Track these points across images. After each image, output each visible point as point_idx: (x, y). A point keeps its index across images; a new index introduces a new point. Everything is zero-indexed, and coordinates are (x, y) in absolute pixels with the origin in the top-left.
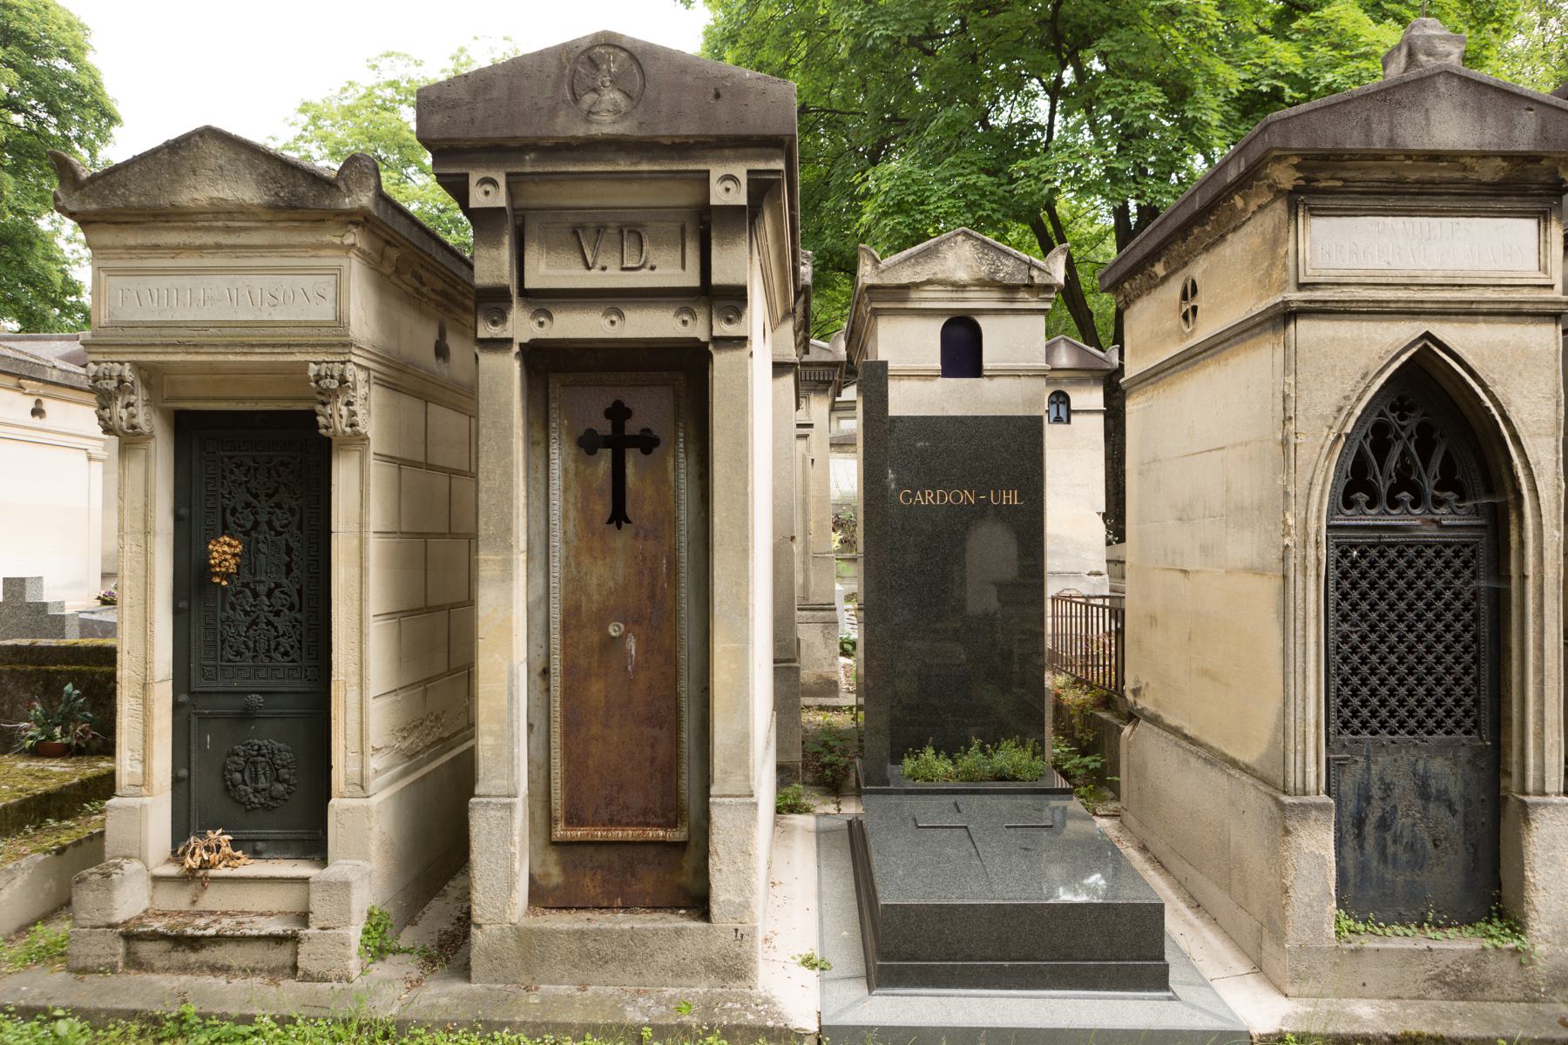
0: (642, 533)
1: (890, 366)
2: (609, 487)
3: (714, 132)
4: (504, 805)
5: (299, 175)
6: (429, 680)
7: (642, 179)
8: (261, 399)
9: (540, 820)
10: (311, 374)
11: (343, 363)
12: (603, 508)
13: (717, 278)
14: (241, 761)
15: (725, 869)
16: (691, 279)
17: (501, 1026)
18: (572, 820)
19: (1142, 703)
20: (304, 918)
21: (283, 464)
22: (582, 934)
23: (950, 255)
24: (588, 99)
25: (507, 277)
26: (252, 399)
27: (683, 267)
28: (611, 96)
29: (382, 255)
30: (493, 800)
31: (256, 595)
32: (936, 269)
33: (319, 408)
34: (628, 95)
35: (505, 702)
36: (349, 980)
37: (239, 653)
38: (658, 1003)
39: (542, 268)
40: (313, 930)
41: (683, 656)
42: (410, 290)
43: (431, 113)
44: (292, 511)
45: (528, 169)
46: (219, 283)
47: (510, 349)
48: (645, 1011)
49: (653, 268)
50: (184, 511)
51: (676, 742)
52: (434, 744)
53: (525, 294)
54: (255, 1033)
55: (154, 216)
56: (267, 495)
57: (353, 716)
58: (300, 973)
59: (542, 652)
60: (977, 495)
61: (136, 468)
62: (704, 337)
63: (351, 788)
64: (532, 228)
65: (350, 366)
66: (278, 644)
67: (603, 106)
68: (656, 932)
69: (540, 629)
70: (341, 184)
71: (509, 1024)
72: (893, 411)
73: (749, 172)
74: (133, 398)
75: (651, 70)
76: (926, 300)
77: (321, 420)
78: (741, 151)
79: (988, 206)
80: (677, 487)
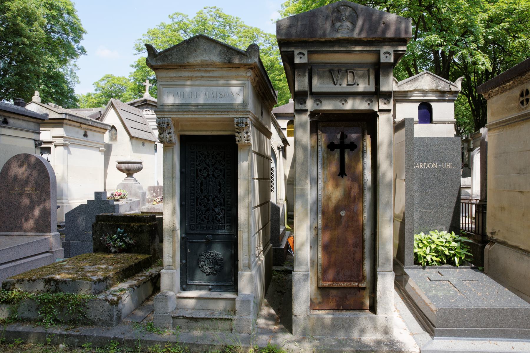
8: (212, 131)
10: (235, 122)
11: (247, 118)
16: (371, 88)
18: (324, 281)
19: (495, 237)
21: (219, 154)
25: (306, 87)
31: (208, 200)
33: (236, 134)
37: (203, 221)
40: (237, 317)
44: (221, 171)
50: (183, 170)
53: (313, 94)
55: (181, 66)
56: (212, 165)
60: (438, 165)
61: (169, 156)
64: (315, 69)
65: (248, 119)
66: (216, 217)
70: (248, 54)
72: (415, 136)
74: (171, 131)
77: (237, 139)
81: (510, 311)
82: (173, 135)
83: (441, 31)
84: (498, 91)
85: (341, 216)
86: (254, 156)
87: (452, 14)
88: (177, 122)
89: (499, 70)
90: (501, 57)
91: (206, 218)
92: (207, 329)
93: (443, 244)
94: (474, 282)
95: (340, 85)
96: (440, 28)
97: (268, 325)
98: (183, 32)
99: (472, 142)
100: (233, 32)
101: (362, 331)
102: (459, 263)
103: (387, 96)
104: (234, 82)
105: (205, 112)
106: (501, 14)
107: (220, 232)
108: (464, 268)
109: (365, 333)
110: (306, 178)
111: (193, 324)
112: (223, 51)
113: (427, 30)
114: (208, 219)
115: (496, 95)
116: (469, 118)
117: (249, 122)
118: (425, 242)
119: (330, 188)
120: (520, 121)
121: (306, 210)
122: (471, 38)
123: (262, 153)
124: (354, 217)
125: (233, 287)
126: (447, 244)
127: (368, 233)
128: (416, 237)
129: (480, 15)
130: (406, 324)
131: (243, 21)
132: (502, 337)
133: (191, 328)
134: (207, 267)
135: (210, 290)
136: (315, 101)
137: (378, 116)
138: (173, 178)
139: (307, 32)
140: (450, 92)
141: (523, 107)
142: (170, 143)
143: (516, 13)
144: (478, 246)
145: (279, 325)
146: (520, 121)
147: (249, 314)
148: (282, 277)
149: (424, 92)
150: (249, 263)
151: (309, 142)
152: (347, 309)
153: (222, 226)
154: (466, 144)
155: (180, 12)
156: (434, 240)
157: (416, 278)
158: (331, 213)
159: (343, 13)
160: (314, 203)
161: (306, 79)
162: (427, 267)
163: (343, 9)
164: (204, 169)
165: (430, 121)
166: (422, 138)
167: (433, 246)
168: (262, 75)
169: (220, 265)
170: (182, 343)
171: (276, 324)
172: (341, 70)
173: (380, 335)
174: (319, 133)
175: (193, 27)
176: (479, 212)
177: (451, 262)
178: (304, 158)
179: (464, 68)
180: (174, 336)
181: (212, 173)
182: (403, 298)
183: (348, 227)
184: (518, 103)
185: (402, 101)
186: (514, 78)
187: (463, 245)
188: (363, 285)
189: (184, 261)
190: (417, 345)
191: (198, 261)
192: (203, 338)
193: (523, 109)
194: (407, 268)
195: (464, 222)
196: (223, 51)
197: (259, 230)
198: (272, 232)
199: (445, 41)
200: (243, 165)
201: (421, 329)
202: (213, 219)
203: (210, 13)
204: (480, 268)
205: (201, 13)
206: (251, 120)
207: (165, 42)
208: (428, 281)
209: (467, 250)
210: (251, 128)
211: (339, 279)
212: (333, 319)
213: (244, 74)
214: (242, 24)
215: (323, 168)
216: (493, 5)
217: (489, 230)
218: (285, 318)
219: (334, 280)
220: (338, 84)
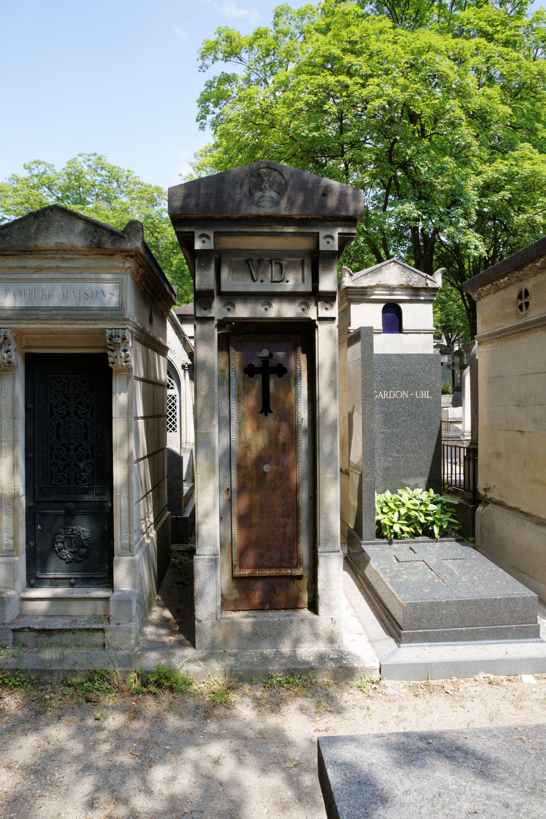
8: (74, 347)
11: (124, 329)
16: (307, 287)
19: (489, 495)
31: (69, 450)
33: (109, 353)
37: (60, 481)
40: (113, 625)
42: (143, 289)
50: (30, 406)
53: (221, 294)
55: (25, 251)
56: (74, 397)
60: (409, 393)
65: (127, 331)
66: (81, 476)
67: (266, 199)
70: (126, 236)
72: (375, 352)
77: (110, 359)
81: (504, 602)
82: (13, 354)
83: (420, 199)
84: (490, 290)
85: (265, 473)
86: (139, 385)
87: (434, 177)
88: (19, 335)
89: (501, 255)
90: (503, 237)
91: (64, 478)
92: (66, 646)
93: (417, 508)
94: (459, 561)
95: (262, 281)
96: (418, 194)
97: (160, 636)
98: (46, 190)
99: (465, 355)
100: (123, 192)
101: (297, 642)
102: (439, 534)
104: (108, 276)
106: (499, 179)
107: (86, 498)
108: (446, 541)
109: (302, 643)
110: (212, 417)
111: (44, 639)
113: (401, 197)
114: (69, 479)
115: (487, 295)
116: (463, 321)
118: (391, 505)
119: (249, 432)
120: (518, 332)
121: (213, 463)
122: (460, 211)
123: (152, 378)
124: (284, 475)
125: (107, 580)
126: (423, 508)
127: (304, 496)
128: (378, 497)
129: (472, 179)
130: (363, 626)
131: (138, 175)
132: (494, 638)
133: (39, 646)
134: (67, 552)
135: (72, 585)
136: (225, 305)
137: (317, 327)
138: (14, 418)
139: (212, 204)
140: (426, 289)
141: (522, 314)
142: (10, 366)
143: (520, 179)
144: (467, 507)
145: (177, 636)
146: (518, 332)
147: (130, 621)
148: (186, 560)
149: (390, 289)
150: (130, 544)
151: (216, 365)
152: (275, 608)
153: (90, 489)
154: (457, 359)
155: (41, 159)
156: (405, 502)
157: (380, 558)
158: (250, 468)
159: (266, 179)
160: (225, 453)
161: (212, 273)
162: (395, 541)
163: (265, 173)
164: (63, 405)
165: (399, 329)
166: (386, 355)
167: (403, 511)
168: (149, 265)
169: (86, 547)
170: (27, 670)
171: (173, 633)
172: (263, 260)
173: (324, 645)
174: (232, 351)
175: (61, 182)
176: (469, 459)
177: (429, 534)
178: (209, 388)
179: (455, 251)
180: (14, 660)
181: (74, 410)
182: (361, 588)
183: (275, 488)
184: (515, 308)
185: (359, 302)
186: (510, 272)
187: (445, 507)
188: (298, 572)
189: (32, 544)
190: (376, 657)
191: (54, 542)
192: (60, 661)
193: (522, 317)
194: (366, 544)
195: (450, 472)
196: (89, 230)
197: (148, 493)
198: (170, 493)
199: (424, 213)
200: (120, 399)
201: (383, 633)
202: (76, 479)
203: (88, 163)
204: (470, 539)
205: (74, 161)
206: (131, 332)
207: (17, 204)
208: (395, 561)
209: (450, 514)
210: (131, 344)
211: (263, 565)
212: (254, 624)
213: (121, 265)
214: (137, 180)
215: (239, 401)
216: (489, 166)
217: (481, 486)
218: (185, 624)
219: (257, 566)
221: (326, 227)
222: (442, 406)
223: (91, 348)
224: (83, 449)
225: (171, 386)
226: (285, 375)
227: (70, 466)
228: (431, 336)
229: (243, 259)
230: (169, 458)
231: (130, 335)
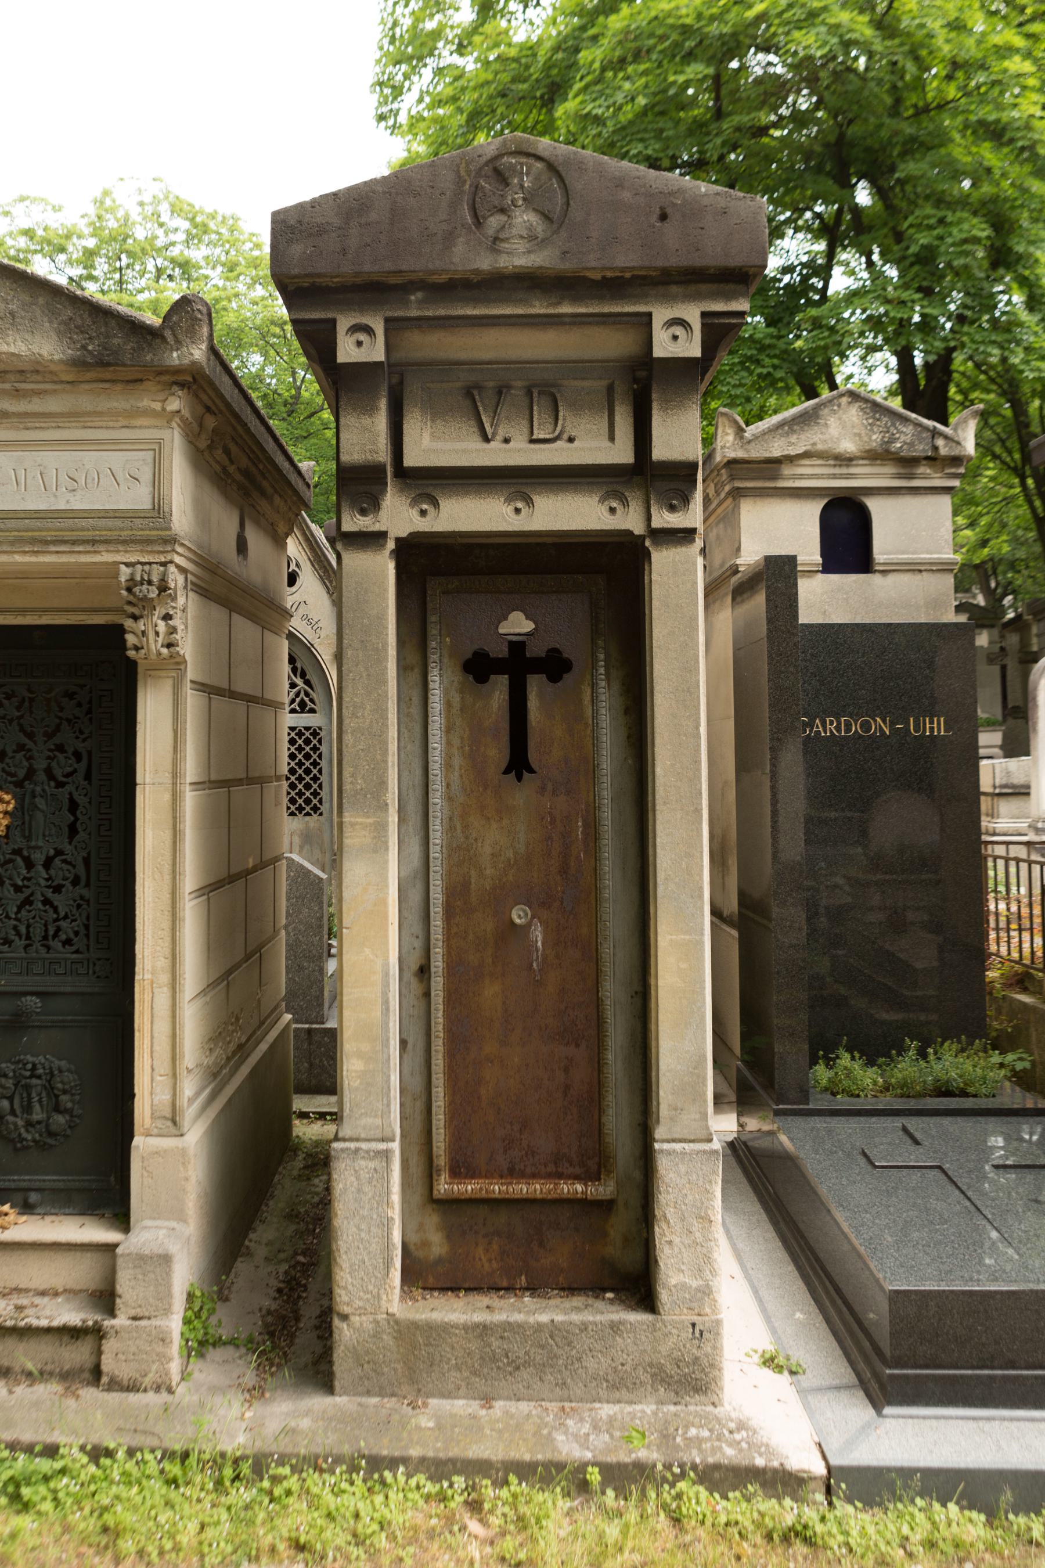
0: (550, 787)
1: (800, 559)
2: (505, 725)
3: (660, 263)
4: (378, 1153)
5: (113, 323)
6: (230, 972)
7: (564, 324)
8: (45, 610)
9: (417, 1170)
11: (164, 564)
12: (498, 753)
13: (660, 452)
14: (9, 1083)
15: (677, 1240)
16: (622, 453)
17: (393, 1463)
18: (459, 1170)
20: (106, 1299)
21: (71, 696)
22: (483, 1330)
23: (833, 422)
24: (494, 222)
26: (33, 610)
27: (612, 438)
28: (525, 218)
29: (201, 425)
30: (364, 1146)
31: (29, 864)
32: (816, 438)
33: (129, 623)
34: (546, 217)
35: (378, 1013)
36: (170, 1391)
38: (596, 1427)
39: (426, 441)
40: (121, 1321)
41: (607, 950)
42: (218, 468)
43: (290, 241)
45: (414, 313)
46: (53, 460)
47: (383, 546)
48: (583, 1441)
49: (571, 440)
51: (598, 1064)
52: (234, 1053)
53: (406, 476)
54: (63, 1471)
57: (162, 1027)
58: (105, 1379)
59: (418, 944)
60: (893, 723)
62: (638, 529)
63: (159, 1123)
64: (413, 389)
65: (172, 568)
67: (514, 231)
68: (584, 1327)
69: (418, 914)
70: (168, 334)
71: (405, 1460)
72: (802, 620)
73: (704, 315)
75: (577, 185)
76: (802, 477)
77: (131, 639)
78: (692, 288)
79: (767, 361)
80: (596, 725)
91: (18, 934)
99: (1035, 630)
103: (675, 481)
105: (12, 543)
112: (79, 322)
114: (28, 938)
117: (175, 579)
137: (648, 555)
155: (25, 194)
161: (381, 422)
196: (79, 322)
202: (45, 938)
206: (182, 570)
213: (157, 406)
220: (499, 438)
221: (669, 299)
222: (982, 752)
223: (84, 610)
224: (64, 861)
225: (310, 705)
226: (565, 676)
227: (31, 903)
228: (949, 580)
229: (458, 384)
230: (292, 881)
231: (181, 579)
